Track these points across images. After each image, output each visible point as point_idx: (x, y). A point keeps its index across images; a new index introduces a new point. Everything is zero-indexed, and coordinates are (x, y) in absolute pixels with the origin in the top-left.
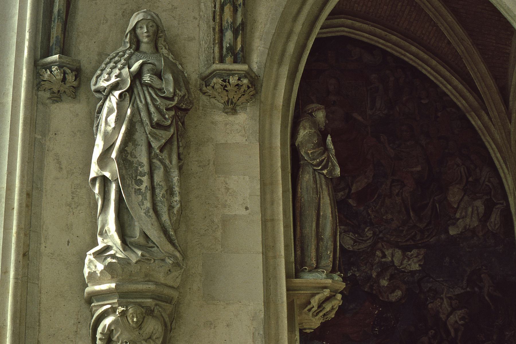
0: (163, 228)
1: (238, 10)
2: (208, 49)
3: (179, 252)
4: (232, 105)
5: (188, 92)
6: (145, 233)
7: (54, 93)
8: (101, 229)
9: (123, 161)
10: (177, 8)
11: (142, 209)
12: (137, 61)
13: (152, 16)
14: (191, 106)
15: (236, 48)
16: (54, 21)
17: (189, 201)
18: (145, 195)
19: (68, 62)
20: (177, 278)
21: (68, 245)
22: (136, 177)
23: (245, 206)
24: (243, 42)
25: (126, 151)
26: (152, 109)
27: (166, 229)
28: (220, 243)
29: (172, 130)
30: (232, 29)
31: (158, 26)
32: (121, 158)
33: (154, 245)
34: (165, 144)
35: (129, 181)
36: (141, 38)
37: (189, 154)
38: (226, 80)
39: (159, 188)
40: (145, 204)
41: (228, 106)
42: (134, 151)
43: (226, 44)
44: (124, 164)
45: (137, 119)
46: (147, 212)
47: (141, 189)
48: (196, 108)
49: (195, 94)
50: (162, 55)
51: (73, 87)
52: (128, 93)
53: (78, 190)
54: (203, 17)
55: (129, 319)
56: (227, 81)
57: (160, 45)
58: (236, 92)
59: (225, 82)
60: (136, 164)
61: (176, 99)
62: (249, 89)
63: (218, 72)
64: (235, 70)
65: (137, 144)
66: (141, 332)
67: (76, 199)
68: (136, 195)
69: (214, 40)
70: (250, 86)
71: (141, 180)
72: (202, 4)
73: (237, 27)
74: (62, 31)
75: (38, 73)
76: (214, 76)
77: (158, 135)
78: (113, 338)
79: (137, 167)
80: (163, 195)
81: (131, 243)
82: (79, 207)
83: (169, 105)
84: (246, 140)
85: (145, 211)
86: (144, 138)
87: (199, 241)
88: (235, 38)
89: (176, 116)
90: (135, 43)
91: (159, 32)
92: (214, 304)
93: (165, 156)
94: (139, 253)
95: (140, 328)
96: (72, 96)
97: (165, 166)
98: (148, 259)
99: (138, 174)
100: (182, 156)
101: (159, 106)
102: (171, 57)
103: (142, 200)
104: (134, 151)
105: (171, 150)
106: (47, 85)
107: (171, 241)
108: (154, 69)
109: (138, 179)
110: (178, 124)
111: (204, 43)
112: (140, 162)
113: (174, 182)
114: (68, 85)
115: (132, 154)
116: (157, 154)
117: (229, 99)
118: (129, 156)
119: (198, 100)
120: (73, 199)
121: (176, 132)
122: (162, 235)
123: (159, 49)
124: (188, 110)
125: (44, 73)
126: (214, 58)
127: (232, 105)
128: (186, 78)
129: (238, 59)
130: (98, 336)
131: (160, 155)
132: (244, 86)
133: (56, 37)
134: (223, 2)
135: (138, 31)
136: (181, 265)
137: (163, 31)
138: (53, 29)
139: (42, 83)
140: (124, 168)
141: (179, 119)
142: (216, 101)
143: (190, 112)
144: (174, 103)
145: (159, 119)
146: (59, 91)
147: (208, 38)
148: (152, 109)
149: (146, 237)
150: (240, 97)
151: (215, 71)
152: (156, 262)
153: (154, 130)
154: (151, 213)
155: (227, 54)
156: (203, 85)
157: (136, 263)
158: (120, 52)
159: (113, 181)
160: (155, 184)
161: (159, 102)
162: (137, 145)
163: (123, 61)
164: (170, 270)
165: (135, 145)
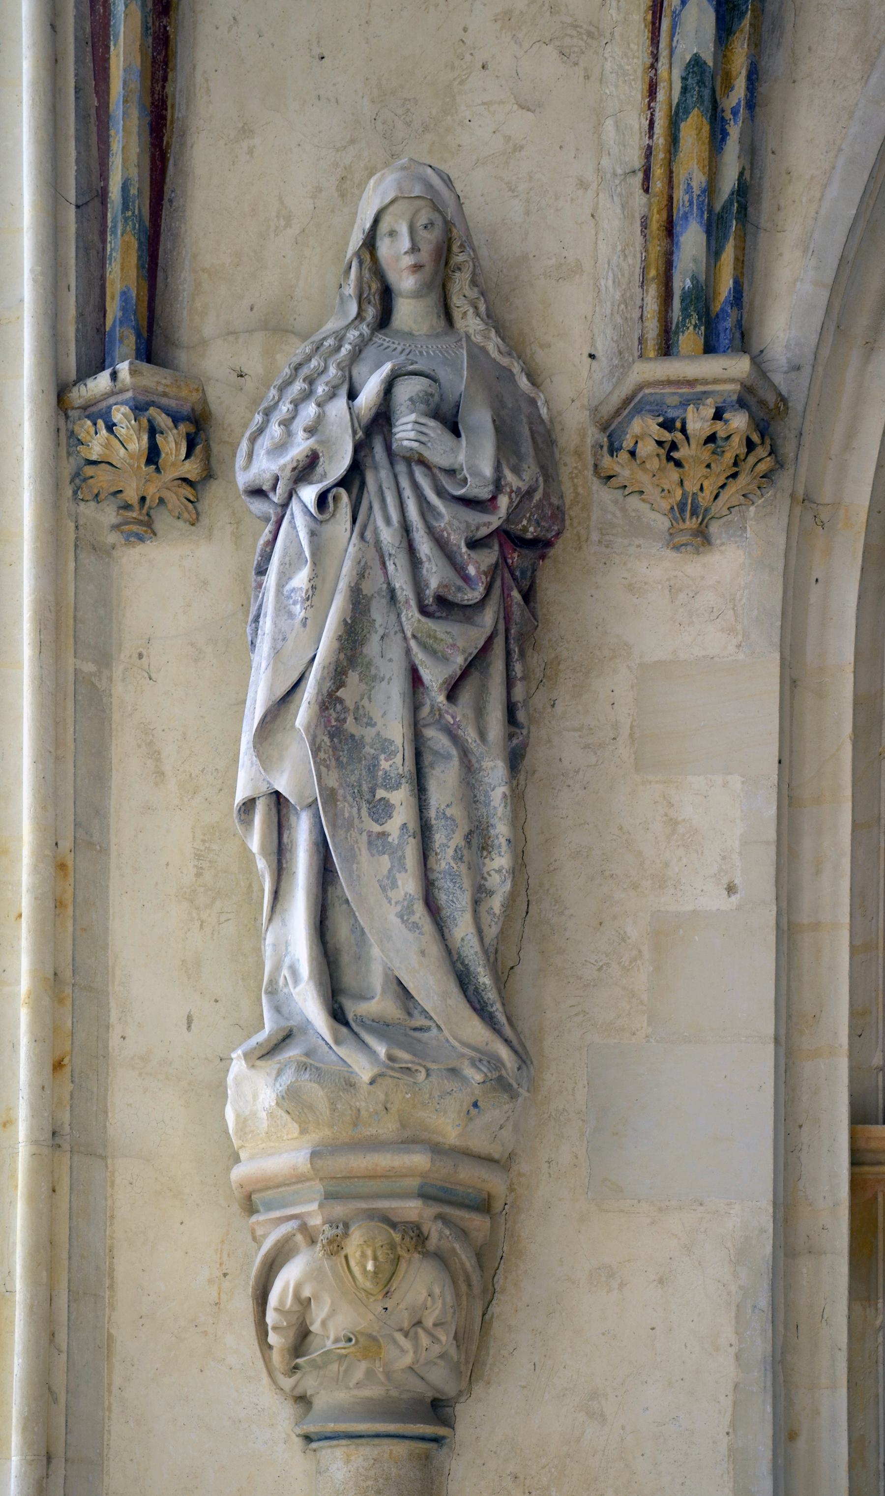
0: (459, 965)
1: (728, 134)
2: (623, 306)
3: (507, 1042)
4: (694, 519)
5: (547, 478)
6: (400, 983)
7: (127, 507)
8: (270, 975)
9: (332, 736)
10: (521, 148)
11: (390, 902)
12: (378, 366)
13: (429, 186)
14: (556, 528)
15: (716, 293)
16: (114, 232)
17: (552, 869)
18: (400, 853)
19: (161, 389)
20: (501, 1127)
21: (189, 1028)
22: (373, 791)
23: (725, 881)
24: (741, 264)
25: (340, 701)
26: (425, 547)
27: (466, 966)
28: (645, 1008)
29: (488, 618)
30: (703, 213)
31: (448, 226)
32: (326, 727)
33: (428, 1023)
34: (465, 674)
35: (351, 807)
36: (392, 277)
37: (553, 706)
38: (673, 421)
39: (445, 827)
40: (400, 883)
41: (684, 521)
42: (365, 702)
43: (681, 282)
44: (334, 748)
45: (374, 585)
46: (404, 915)
47: (389, 835)
48: (579, 539)
49: (575, 487)
50: (464, 339)
51: (185, 480)
52: (349, 491)
53: (215, 847)
54: (609, 176)
55: (352, 1263)
56: (678, 424)
57: (457, 301)
58: (708, 466)
59: (670, 431)
60: (372, 748)
61: (503, 502)
62: (753, 453)
63: (651, 394)
64: (705, 382)
65: (375, 676)
66: (389, 1304)
67: (208, 876)
68: (373, 855)
69: (644, 271)
70: (756, 438)
71: (388, 801)
72: (609, 124)
73: (723, 208)
74: (140, 266)
75: (72, 434)
76: (638, 410)
77: (442, 640)
78: (312, 1324)
79: (375, 758)
80: (456, 851)
81: (362, 1023)
82: (218, 903)
83: (478, 529)
84: (739, 646)
85: (399, 908)
86: (395, 651)
87: (579, 1004)
88: (714, 253)
89: (506, 570)
90: (377, 297)
91: (455, 249)
92: (622, 1211)
93: (464, 715)
94: (381, 1050)
95: (387, 1293)
96: (186, 515)
97: (465, 753)
98: (408, 1069)
99: (380, 780)
100: (521, 716)
101: (445, 534)
102: (493, 345)
103: (390, 871)
104: (365, 702)
105: (482, 691)
106: (102, 478)
107: (481, 1010)
108: (432, 395)
109: (378, 797)
110: (509, 595)
111: (610, 282)
112: (386, 740)
113: (492, 804)
114: (170, 474)
115: (361, 711)
116: (440, 710)
117: (684, 495)
118: (350, 719)
119: (586, 508)
120: (198, 875)
121: (501, 627)
122: (453, 988)
123: (457, 314)
124: (548, 544)
125: (88, 433)
126: (641, 341)
127: (694, 519)
128: (542, 421)
129: (722, 335)
130: (271, 1317)
131: (447, 712)
132: (736, 440)
133: (123, 293)
134: (678, 105)
135: (384, 248)
136: (515, 1086)
137: (468, 244)
138: (110, 264)
139: (89, 470)
140: (333, 763)
141: (515, 578)
142: (644, 507)
143: (556, 551)
144: (494, 521)
145: (445, 583)
146: (143, 499)
147: (624, 265)
148: (425, 547)
149: (404, 993)
150: (723, 486)
151: (640, 387)
152: (433, 1078)
153: (429, 624)
154: (418, 915)
155: (684, 319)
156: (601, 447)
157: (371, 1083)
158: (325, 339)
159: (302, 809)
160: (432, 813)
161: (447, 518)
162: (374, 678)
163: (332, 371)
164: (475, 1105)
165: (370, 679)
